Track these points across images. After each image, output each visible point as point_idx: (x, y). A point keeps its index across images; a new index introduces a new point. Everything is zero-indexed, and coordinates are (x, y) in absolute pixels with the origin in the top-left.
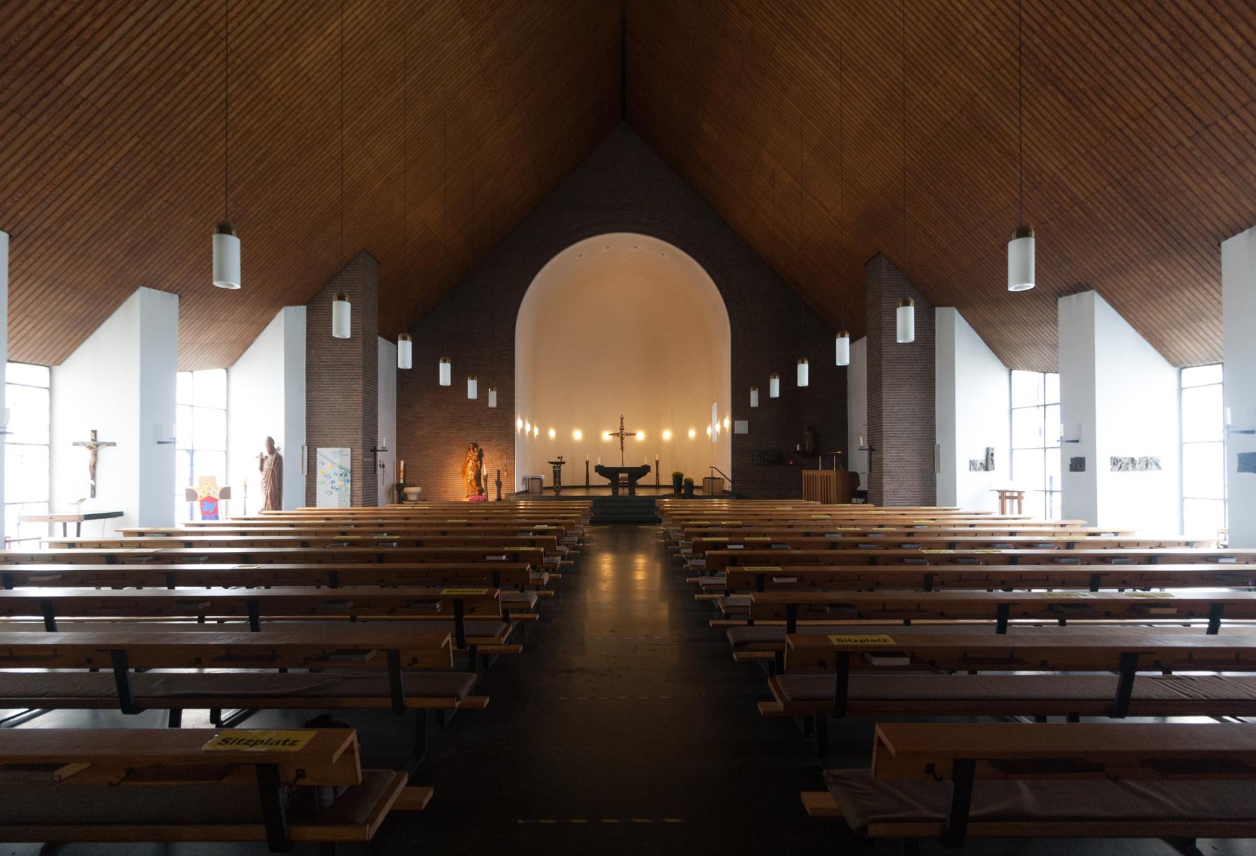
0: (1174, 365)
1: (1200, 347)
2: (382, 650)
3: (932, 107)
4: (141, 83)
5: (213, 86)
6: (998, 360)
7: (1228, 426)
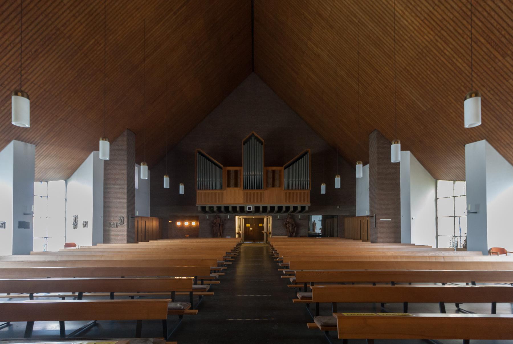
0: (434, 178)
1: (455, 170)
2: (130, 296)
3: (344, 18)
4: (43, 12)
5: (428, 67)
6: (429, 174)
7: (469, 211)
